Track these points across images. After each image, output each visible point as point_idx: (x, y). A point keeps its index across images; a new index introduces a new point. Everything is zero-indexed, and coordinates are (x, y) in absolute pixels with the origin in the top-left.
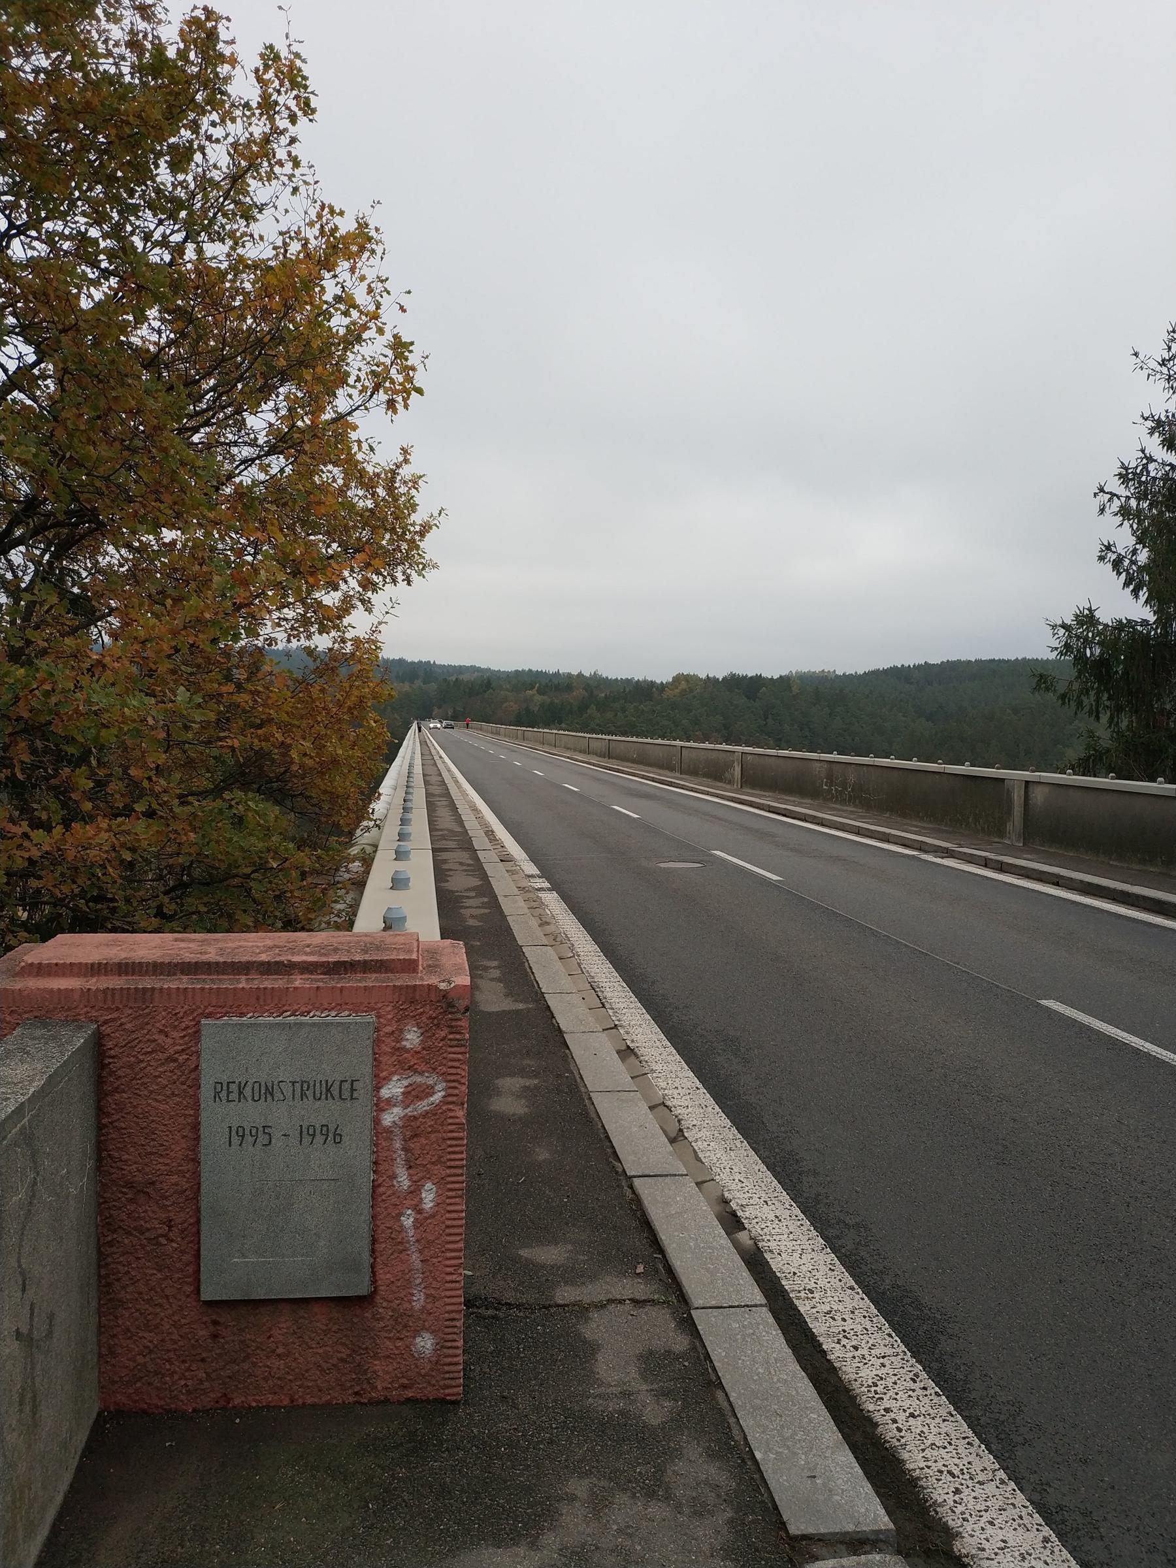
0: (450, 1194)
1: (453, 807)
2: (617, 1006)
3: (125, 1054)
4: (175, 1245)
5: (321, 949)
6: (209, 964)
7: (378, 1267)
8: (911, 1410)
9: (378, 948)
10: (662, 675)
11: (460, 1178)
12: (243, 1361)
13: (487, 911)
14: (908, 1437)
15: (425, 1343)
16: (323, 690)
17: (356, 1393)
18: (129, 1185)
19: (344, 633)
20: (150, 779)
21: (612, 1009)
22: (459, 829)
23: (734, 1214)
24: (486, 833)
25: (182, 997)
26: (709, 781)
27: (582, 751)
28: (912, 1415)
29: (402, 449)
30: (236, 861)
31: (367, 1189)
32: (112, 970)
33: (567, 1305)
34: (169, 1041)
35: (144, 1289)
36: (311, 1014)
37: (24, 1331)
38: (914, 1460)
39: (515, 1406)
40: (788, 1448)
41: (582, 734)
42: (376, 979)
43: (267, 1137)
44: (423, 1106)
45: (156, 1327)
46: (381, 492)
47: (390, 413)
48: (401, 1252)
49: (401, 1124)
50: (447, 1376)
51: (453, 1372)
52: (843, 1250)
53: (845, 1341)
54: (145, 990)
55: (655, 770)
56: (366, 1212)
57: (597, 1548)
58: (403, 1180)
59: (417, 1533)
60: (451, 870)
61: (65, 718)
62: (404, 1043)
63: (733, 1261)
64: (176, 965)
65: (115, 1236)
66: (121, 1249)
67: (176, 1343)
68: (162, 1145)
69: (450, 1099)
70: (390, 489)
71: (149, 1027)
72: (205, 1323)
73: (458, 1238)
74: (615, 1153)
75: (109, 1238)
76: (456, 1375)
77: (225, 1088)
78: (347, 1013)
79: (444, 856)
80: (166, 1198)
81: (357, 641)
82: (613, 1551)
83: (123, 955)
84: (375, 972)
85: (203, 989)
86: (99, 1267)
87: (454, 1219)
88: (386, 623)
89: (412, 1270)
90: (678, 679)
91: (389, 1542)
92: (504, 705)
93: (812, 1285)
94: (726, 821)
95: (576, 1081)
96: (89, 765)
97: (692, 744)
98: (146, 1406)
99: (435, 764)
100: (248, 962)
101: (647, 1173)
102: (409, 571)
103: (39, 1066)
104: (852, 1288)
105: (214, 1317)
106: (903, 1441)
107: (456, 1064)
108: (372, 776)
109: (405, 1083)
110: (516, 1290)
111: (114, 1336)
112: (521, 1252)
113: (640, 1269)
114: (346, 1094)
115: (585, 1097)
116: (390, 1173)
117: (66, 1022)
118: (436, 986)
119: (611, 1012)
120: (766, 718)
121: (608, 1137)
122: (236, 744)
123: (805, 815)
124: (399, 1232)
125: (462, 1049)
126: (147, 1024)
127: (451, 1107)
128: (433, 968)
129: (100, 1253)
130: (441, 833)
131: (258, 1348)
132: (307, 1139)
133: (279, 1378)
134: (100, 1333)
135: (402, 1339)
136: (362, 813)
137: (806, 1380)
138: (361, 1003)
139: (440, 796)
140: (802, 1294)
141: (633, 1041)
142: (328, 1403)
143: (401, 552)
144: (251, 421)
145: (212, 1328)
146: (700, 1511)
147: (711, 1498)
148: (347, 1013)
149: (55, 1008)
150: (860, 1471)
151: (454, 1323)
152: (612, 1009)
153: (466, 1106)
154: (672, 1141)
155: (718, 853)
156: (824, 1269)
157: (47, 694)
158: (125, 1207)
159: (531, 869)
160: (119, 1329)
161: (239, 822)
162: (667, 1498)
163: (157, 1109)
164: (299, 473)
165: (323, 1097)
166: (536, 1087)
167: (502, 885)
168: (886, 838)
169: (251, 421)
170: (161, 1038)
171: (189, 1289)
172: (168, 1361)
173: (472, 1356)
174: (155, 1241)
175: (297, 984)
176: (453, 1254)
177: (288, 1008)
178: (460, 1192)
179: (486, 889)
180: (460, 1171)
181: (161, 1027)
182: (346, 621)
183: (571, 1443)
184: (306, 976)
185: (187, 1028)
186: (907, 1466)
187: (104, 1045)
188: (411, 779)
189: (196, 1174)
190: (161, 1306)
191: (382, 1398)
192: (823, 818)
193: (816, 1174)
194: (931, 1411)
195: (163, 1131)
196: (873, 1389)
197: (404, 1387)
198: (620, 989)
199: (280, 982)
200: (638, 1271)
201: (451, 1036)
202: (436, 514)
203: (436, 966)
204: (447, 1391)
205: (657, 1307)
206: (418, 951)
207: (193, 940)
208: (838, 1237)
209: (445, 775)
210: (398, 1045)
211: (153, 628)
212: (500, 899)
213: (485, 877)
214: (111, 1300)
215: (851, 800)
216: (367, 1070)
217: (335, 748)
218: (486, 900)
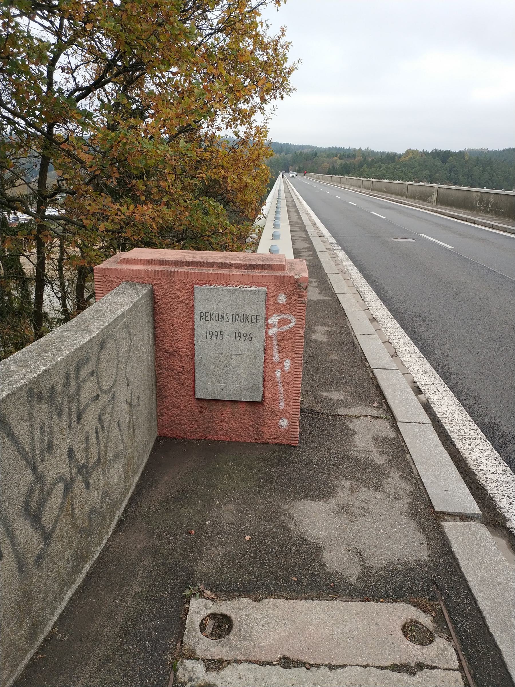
0: (296, 364)
1: (298, 212)
2: (370, 300)
5: (243, 259)
6: (197, 262)
7: (265, 391)
8: (493, 471)
9: (268, 260)
10: (400, 150)
11: (301, 359)
12: (212, 422)
13: (312, 258)
14: (490, 481)
15: (284, 423)
16: (242, 151)
17: (256, 439)
18: (167, 351)
19: (251, 124)
20: (169, 186)
22: (300, 222)
23: (418, 388)
24: (312, 224)
25: (186, 275)
26: (420, 201)
27: (359, 187)
28: (493, 473)
29: (282, 28)
30: (205, 228)
31: (262, 360)
34: (182, 294)
37: (129, 401)
38: (492, 490)
39: (320, 451)
40: (437, 479)
41: (360, 178)
44: (286, 328)
45: (179, 407)
46: (271, 51)
47: (277, 6)
49: (276, 335)
52: (467, 406)
53: (465, 442)
54: (171, 272)
55: (394, 196)
56: (261, 369)
57: (353, 506)
58: (277, 357)
61: (133, 156)
62: (279, 301)
63: (417, 405)
67: (186, 413)
69: (298, 326)
70: (275, 50)
71: (173, 288)
73: (299, 382)
76: (296, 436)
77: (204, 315)
78: (255, 286)
81: (257, 128)
83: (161, 257)
85: (195, 273)
86: (156, 382)
88: (271, 118)
90: (408, 152)
92: (323, 165)
93: (452, 418)
94: (427, 220)
96: (143, 179)
97: (413, 183)
100: (213, 262)
102: (282, 92)
103: (130, 299)
104: (470, 421)
106: (488, 482)
107: (301, 311)
109: (279, 318)
111: (162, 409)
112: (323, 393)
114: (254, 321)
115: (353, 336)
117: (139, 283)
119: (366, 303)
120: (451, 172)
121: (363, 352)
122: (204, 176)
123: (467, 218)
125: (304, 305)
126: (172, 286)
127: (298, 329)
128: (292, 269)
129: (156, 377)
132: (238, 338)
134: (157, 407)
136: (258, 211)
137: (447, 454)
140: (447, 422)
142: (245, 442)
143: (279, 83)
144: (209, 15)
145: (200, 409)
146: (397, 498)
147: (402, 494)
148: (255, 286)
150: (469, 491)
151: (296, 416)
154: (392, 356)
155: (422, 235)
156: (458, 413)
157: (125, 144)
159: (332, 240)
161: (206, 213)
162: (383, 491)
164: (233, 42)
165: (245, 321)
166: (332, 331)
167: (319, 246)
168: (505, 230)
169: (209, 15)
170: (178, 293)
171: (191, 393)
175: (234, 272)
176: (297, 389)
180: (300, 356)
182: (252, 119)
184: (237, 270)
185: (188, 289)
186: (489, 492)
188: (279, 203)
189: (193, 349)
190: (180, 399)
192: (475, 220)
193: (457, 374)
194: (502, 472)
196: (476, 461)
197: (275, 438)
201: (299, 299)
202: (296, 62)
203: (293, 269)
207: (189, 253)
208: (465, 400)
209: (294, 197)
211: (169, 113)
212: (318, 253)
213: (311, 243)
214: (160, 395)
215: (490, 212)
216: (262, 311)
217: (247, 179)
218: (311, 253)
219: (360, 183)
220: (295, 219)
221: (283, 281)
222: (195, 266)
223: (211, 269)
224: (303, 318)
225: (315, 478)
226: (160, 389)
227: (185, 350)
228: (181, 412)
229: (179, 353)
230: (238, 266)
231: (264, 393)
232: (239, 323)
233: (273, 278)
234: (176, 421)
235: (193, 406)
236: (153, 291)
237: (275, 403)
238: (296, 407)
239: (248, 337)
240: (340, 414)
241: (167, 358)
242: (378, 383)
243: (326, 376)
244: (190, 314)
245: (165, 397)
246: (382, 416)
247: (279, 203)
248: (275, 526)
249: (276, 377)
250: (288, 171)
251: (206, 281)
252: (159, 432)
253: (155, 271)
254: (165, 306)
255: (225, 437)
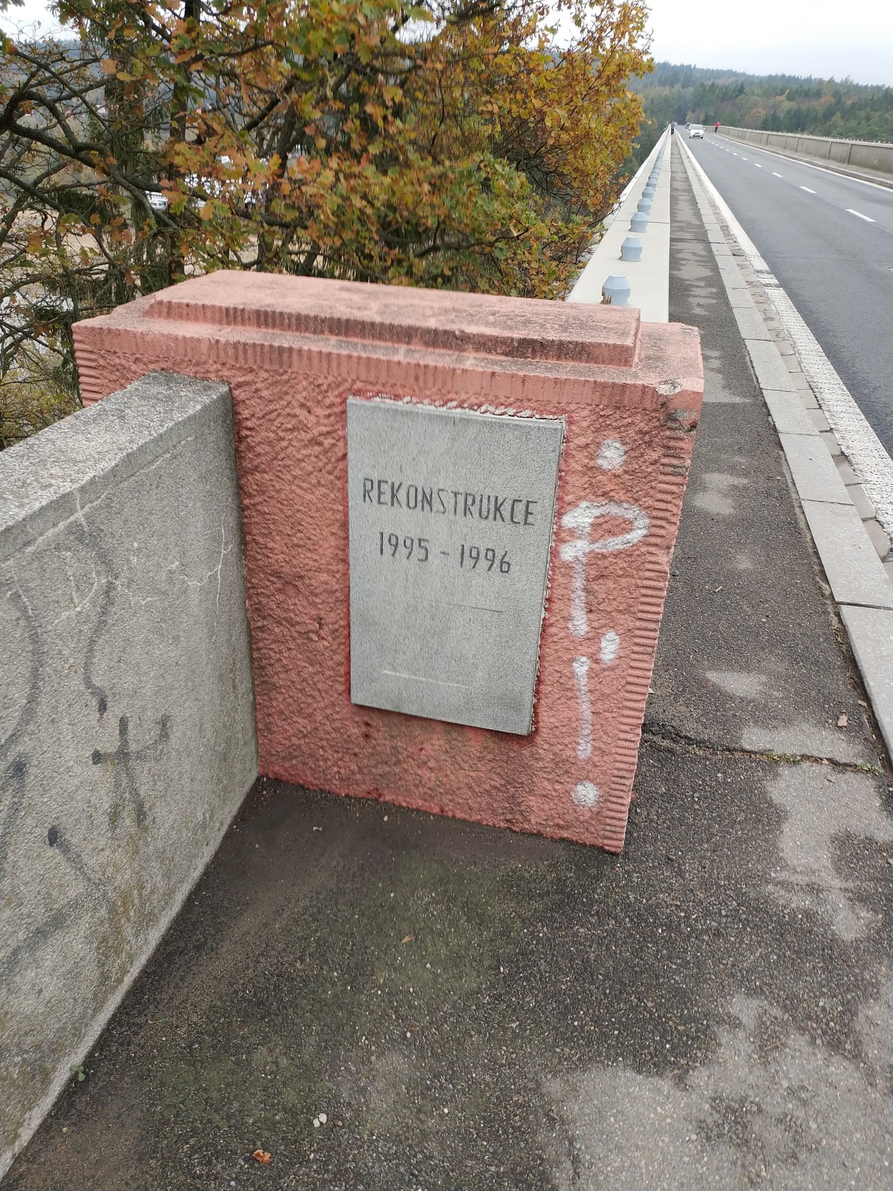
0: (636, 649)
1: (694, 202)
2: (835, 409)
3: (264, 427)
4: (326, 644)
5: (508, 320)
6: (363, 324)
7: (542, 710)
9: (583, 325)
11: (652, 634)
12: (395, 764)
13: (714, 301)
17: (508, 821)
18: (277, 574)
21: (829, 411)
24: (722, 227)
25: (325, 364)
30: (480, 226)
32: (249, 319)
33: (755, 753)
34: (312, 419)
35: (295, 678)
36: (483, 409)
39: (680, 874)
42: (574, 371)
43: (423, 551)
44: (615, 543)
45: (310, 715)
48: (570, 699)
50: (608, 828)
51: (615, 826)
54: (281, 349)
56: (531, 652)
57: (760, 1110)
58: (580, 624)
59: (547, 1023)
60: (684, 259)
62: (600, 462)
64: (323, 321)
65: (265, 623)
66: (272, 637)
68: (309, 539)
69: (653, 540)
71: (288, 398)
72: (357, 722)
73: (640, 697)
74: (823, 572)
75: (260, 624)
77: (376, 486)
78: (528, 412)
79: (680, 246)
80: (316, 595)
82: (780, 1121)
84: (573, 359)
85: (350, 357)
86: (251, 650)
87: (638, 677)
89: (581, 719)
91: (514, 1025)
95: (787, 486)
98: (301, 782)
99: (682, 163)
100: (410, 328)
101: (857, 601)
105: (366, 719)
107: (668, 497)
108: (622, 155)
109: (597, 512)
110: (698, 721)
111: (269, 715)
113: (843, 721)
114: (519, 517)
115: (796, 504)
116: (566, 614)
118: (654, 390)
119: (827, 414)
124: (570, 678)
125: (679, 480)
126: (286, 393)
127: (652, 549)
128: (654, 361)
130: (679, 224)
131: (408, 757)
132: (468, 562)
133: (429, 788)
135: (561, 783)
138: (549, 402)
139: (683, 191)
141: (848, 447)
142: (479, 823)
145: (364, 729)
148: (528, 412)
149: (183, 361)
151: (622, 781)
152: (829, 411)
153: (672, 550)
158: (273, 595)
159: (760, 264)
160: (274, 710)
162: (857, 1056)
163: (303, 498)
165: (491, 516)
166: (746, 488)
167: (731, 277)
170: (302, 413)
171: (341, 688)
172: (322, 747)
173: (641, 795)
174: (305, 635)
177: (455, 396)
178: (650, 650)
179: (715, 281)
180: (653, 626)
181: (302, 401)
183: (741, 942)
184: (482, 355)
185: (331, 406)
187: (240, 414)
189: (346, 574)
190: (313, 697)
191: (535, 832)
195: (309, 524)
198: (839, 392)
199: (448, 359)
200: (840, 724)
201: (665, 460)
203: (658, 358)
204: (606, 842)
205: (861, 775)
206: (636, 335)
207: (358, 291)
210: (592, 463)
212: (729, 291)
213: (715, 268)
214: (265, 682)
217: (590, 121)
218: (714, 290)
219: (824, 149)
220: (686, 214)
221: (621, 401)
222: (355, 335)
223: (403, 348)
224: (673, 519)
225: (657, 977)
226: (262, 668)
227: (324, 577)
228: (316, 729)
229: (307, 581)
230: (485, 344)
231: (536, 713)
232: (474, 520)
233: (588, 389)
234: (305, 749)
235: (346, 719)
236: (234, 405)
237: (566, 741)
238: (625, 759)
239: (497, 562)
240: (748, 747)
241: (279, 590)
242: (850, 649)
243: (720, 619)
244: (338, 478)
245: (275, 687)
246: (860, 762)
247: (656, 176)
248: (513, 1170)
249: (573, 675)
250: (682, 122)
251: (384, 385)
252: (262, 766)
253: (236, 345)
254: (268, 449)
255: (426, 804)
